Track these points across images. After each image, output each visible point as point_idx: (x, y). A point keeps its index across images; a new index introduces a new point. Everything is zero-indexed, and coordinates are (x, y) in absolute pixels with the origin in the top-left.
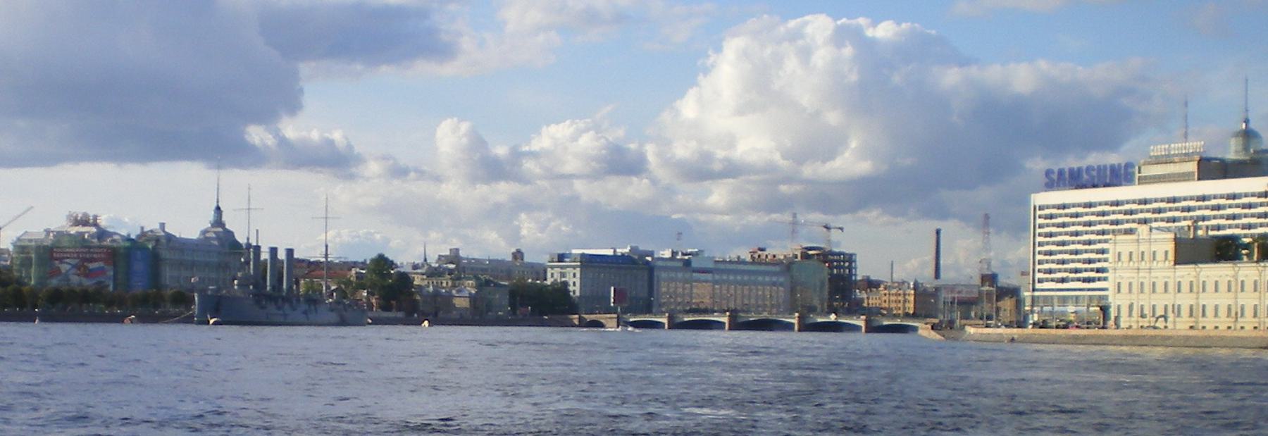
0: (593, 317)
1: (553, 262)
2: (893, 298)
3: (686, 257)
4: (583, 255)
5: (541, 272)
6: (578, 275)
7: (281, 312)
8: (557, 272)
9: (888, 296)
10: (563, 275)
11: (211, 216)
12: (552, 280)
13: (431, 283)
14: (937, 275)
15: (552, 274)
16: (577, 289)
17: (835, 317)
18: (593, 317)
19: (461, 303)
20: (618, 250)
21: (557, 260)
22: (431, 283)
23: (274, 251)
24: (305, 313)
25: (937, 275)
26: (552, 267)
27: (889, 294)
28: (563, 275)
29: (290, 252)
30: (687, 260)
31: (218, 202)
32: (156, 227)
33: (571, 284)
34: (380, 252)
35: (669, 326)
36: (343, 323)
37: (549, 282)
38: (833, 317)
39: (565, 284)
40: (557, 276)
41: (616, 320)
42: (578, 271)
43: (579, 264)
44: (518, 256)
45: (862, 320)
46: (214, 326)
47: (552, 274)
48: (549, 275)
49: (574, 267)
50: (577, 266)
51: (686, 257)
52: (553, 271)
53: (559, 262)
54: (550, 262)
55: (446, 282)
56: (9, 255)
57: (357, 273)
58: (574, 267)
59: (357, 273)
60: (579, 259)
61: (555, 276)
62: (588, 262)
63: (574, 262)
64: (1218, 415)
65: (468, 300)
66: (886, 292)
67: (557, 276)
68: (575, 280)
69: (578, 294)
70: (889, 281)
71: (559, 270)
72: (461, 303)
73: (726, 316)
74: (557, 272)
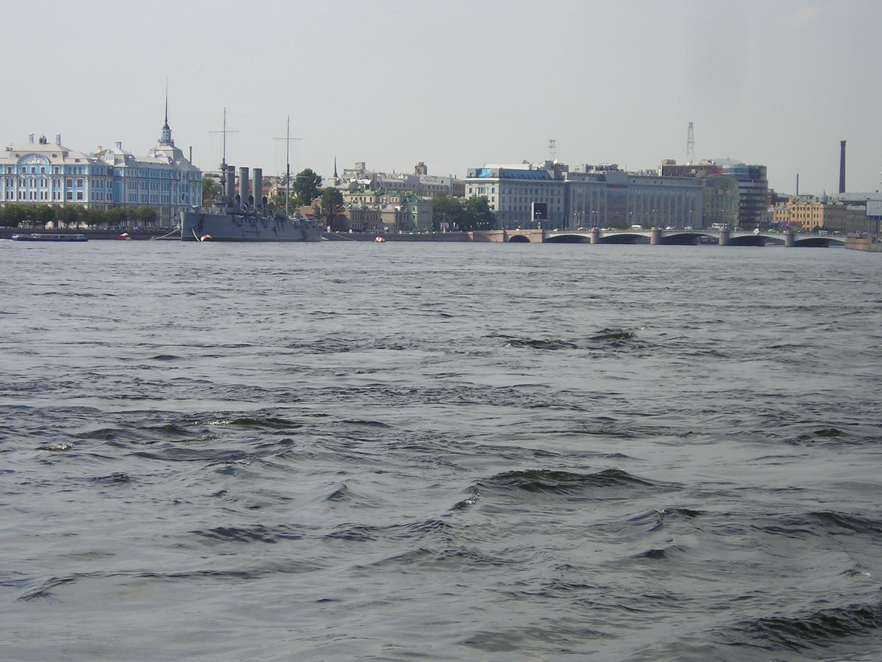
0: (517, 232)
1: (471, 177)
2: (803, 212)
3: (601, 172)
4: (501, 170)
5: (458, 188)
6: (497, 190)
7: (254, 230)
8: (475, 187)
9: (796, 210)
10: (481, 190)
11: (160, 134)
12: (471, 195)
13: (358, 198)
14: (842, 189)
15: (471, 190)
16: (496, 204)
17: (758, 232)
18: (517, 232)
19: (389, 219)
20: (534, 165)
21: (475, 175)
22: (358, 198)
23: (245, 170)
24: (274, 230)
25: (842, 189)
26: (470, 183)
27: (798, 208)
28: (481, 190)
29: (258, 172)
30: (601, 175)
31: (166, 121)
32: (373, 171)
33: (490, 199)
34: (308, 168)
35: (595, 240)
36: (304, 239)
37: (468, 196)
38: (756, 232)
39: (485, 200)
40: (475, 191)
41: (541, 235)
42: (497, 187)
43: (497, 179)
44: (422, 169)
45: (785, 234)
46: (205, 242)
47: (471, 190)
48: (467, 190)
49: (493, 183)
50: (497, 182)
51: (601, 172)
52: (470, 187)
53: (477, 177)
54: (468, 177)
55: (368, 197)
56: (473, 206)
57: (278, 189)
58: (493, 183)
59: (278, 189)
60: (498, 175)
61: (474, 191)
62: (506, 176)
63: (493, 177)
64: (147, 357)
65: (394, 215)
66: (794, 206)
67: (475, 191)
68: (493, 195)
69: (496, 209)
70: (796, 195)
71: (477, 185)
72: (389, 219)
73: (651, 232)
74: (475, 187)
